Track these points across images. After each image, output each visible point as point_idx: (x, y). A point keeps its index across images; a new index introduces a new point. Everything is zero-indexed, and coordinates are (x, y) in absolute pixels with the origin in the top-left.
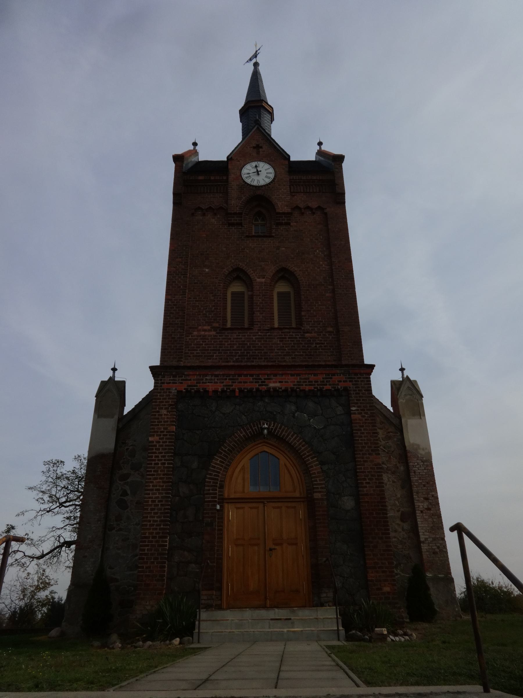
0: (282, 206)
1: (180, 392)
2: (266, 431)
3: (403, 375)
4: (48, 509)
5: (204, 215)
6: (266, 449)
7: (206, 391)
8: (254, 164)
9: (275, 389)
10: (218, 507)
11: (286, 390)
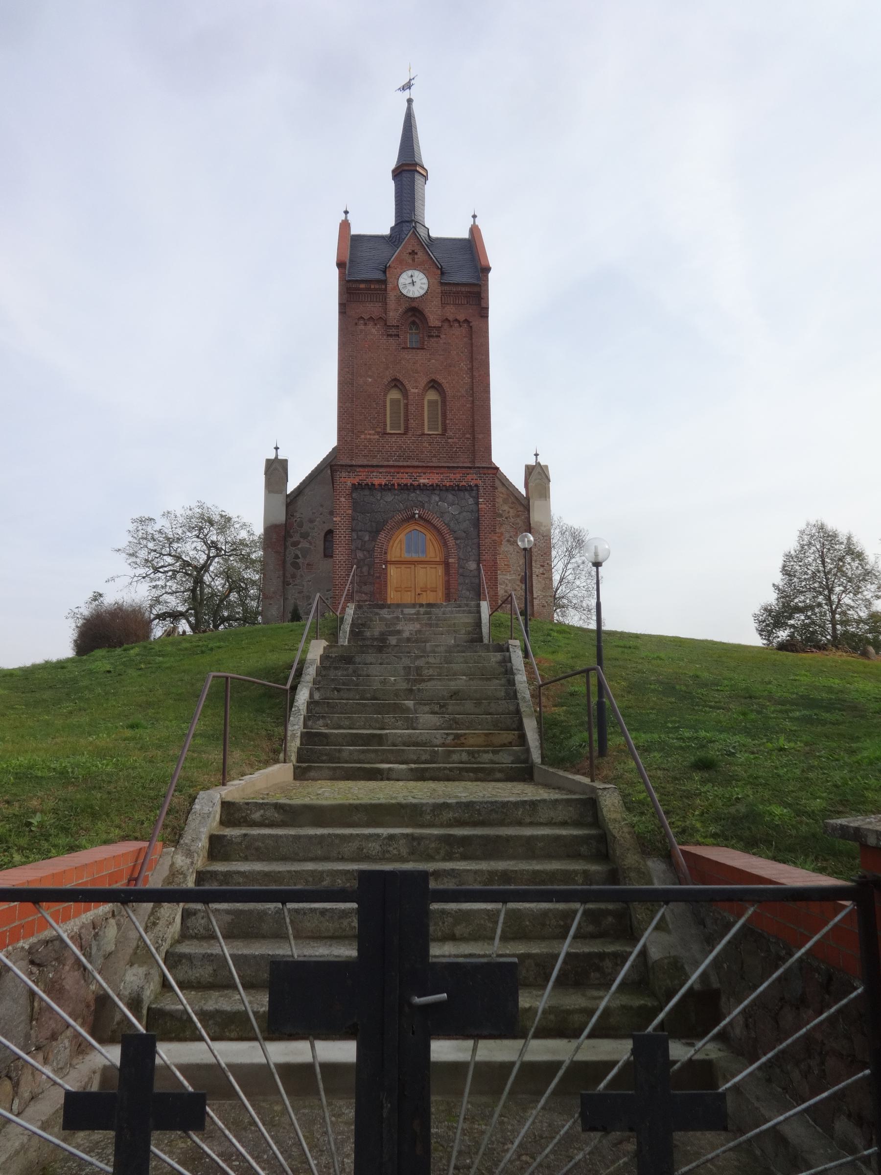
0: (433, 320)
1: (353, 485)
2: (417, 516)
3: (536, 460)
4: (144, 575)
5: (365, 324)
6: (416, 527)
7: (373, 485)
8: (410, 273)
9: (424, 485)
10: (384, 567)
11: (432, 485)
